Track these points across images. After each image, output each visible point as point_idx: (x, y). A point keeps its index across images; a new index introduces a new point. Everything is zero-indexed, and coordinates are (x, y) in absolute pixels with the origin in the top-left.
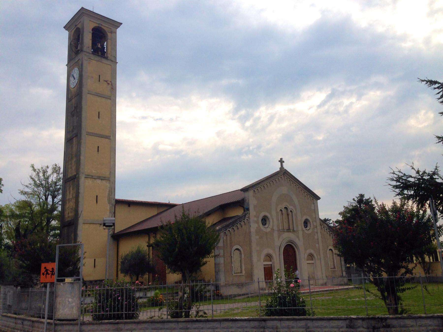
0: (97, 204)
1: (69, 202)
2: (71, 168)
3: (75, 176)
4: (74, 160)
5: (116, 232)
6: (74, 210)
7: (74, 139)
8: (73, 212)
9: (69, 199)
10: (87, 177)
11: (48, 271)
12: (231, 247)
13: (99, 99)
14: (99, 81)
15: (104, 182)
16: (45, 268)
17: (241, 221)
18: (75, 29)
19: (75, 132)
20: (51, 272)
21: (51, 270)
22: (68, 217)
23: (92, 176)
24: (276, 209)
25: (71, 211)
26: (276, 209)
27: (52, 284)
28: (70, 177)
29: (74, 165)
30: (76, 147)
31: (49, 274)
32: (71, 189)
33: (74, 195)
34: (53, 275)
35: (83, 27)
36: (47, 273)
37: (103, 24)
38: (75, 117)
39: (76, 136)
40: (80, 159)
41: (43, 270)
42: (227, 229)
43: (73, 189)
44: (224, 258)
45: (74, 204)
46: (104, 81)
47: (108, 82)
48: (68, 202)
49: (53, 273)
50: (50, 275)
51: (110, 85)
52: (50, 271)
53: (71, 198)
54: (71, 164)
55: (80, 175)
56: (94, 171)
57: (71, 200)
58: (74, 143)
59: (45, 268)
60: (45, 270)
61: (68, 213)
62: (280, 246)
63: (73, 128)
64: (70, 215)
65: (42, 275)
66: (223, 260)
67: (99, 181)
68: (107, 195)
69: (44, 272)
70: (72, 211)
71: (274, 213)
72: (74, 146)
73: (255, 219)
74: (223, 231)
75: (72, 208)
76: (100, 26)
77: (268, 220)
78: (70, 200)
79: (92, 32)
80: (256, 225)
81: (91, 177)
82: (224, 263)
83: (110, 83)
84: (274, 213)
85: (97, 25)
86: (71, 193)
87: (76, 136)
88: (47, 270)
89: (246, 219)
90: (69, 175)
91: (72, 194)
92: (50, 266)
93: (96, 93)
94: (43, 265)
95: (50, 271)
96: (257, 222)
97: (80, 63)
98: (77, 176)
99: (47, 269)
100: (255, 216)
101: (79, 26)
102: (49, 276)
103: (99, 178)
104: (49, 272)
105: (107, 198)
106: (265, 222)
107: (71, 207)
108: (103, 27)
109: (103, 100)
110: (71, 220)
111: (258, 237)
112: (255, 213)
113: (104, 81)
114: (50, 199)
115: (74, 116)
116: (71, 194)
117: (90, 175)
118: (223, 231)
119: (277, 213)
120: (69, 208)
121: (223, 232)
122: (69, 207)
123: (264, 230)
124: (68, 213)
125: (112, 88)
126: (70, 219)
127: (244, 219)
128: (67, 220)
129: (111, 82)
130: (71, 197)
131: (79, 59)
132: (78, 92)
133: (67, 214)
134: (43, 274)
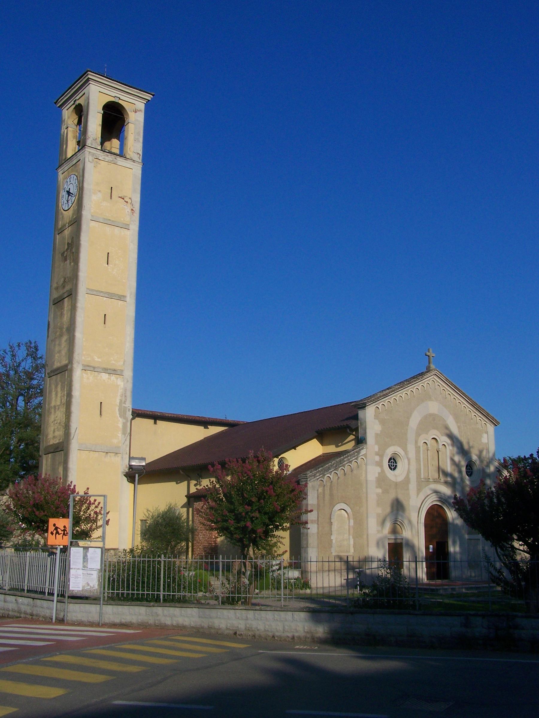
0: (101, 417)
1: (55, 412)
2: (59, 352)
3: (66, 366)
4: (65, 338)
5: (186, 482)
6: (63, 426)
7: (66, 300)
8: (62, 429)
9: (55, 407)
10: (87, 368)
11: (58, 529)
12: (332, 506)
13: (108, 229)
14: (111, 198)
15: (113, 377)
16: (54, 525)
17: (351, 462)
18: (74, 106)
19: (68, 288)
20: (62, 531)
21: (63, 529)
22: (54, 437)
23: (94, 368)
24: (416, 442)
25: (59, 427)
26: (416, 442)
27: (65, 550)
28: (58, 369)
29: (65, 347)
30: (69, 314)
31: (59, 534)
32: (59, 387)
33: (64, 401)
34: (65, 535)
35: (88, 103)
36: (57, 533)
37: (122, 97)
38: (68, 261)
39: (70, 295)
40: (74, 336)
41: (51, 528)
42: (324, 475)
43: (61, 390)
44: (318, 524)
45: (64, 416)
46: (119, 197)
47: (126, 199)
48: (53, 411)
49: (66, 532)
50: (62, 534)
51: (129, 204)
52: (61, 530)
53: (59, 406)
54: (60, 345)
55: (75, 365)
56: (96, 359)
57: (59, 408)
58: (65, 308)
59: (54, 525)
60: (54, 527)
61: (54, 431)
62: (429, 495)
63: (64, 281)
64: (57, 433)
65: (50, 535)
66: (316, 528)
67: (105, 376)
68: (118, 401)
69: (53, 531)
70: (60, 428)
71: (411, 448)
72: (65, 312)
73: (377, 458)
74: (318, 478)
75: (60, 423)
76: (117, 100)
77: (399, 458)
78: (57, 407)
79: (102, 112)
80: (378, 469)
81: (92, 369)
82: (318, 533)
83: (129, 201)
84: (411, 448)
85: (113, 99)
86: (59, 395)
87: (70, 295)
88: (56, 528)
89: (359, 458)
90: (55, 363)
91: (61, 397)
92: (62, 523)
93: (104, 219)
94: (52, 521)
95: (61, 530)
96: (380, 464)
97: (81, 167)
98: (69, 367)
99: (56, 527)
100: (377, 454)
101: (81, 101)
102: (59, 537)
103: (106, 370)
104: (60, 532)
105: (117, 408)
106: (395, 464)
107: (59, 422)
108: (121, 102)
109: (117, 230)
110: (58, 443)
111: (379, 491)
112: (376, 448)
113: (119, 197)
114: (21, 402)
115: (66, 261)
116: (59, 399)
117: (91, 367)
118: (318, 478)
119: (418, 449)
120: (56, 422)
121: (318, 479)
122: (55, 420)
123: (393, 479)
124: (54, 431)
125: (132, 210)
126: (57, 441)
127: (356, 459)
128: (51, 443)
129: (130, 199)
130: (58, 403)
131: (80, 160)
132: (75, 217)
133: (52, 433)
134: (52, 533)
